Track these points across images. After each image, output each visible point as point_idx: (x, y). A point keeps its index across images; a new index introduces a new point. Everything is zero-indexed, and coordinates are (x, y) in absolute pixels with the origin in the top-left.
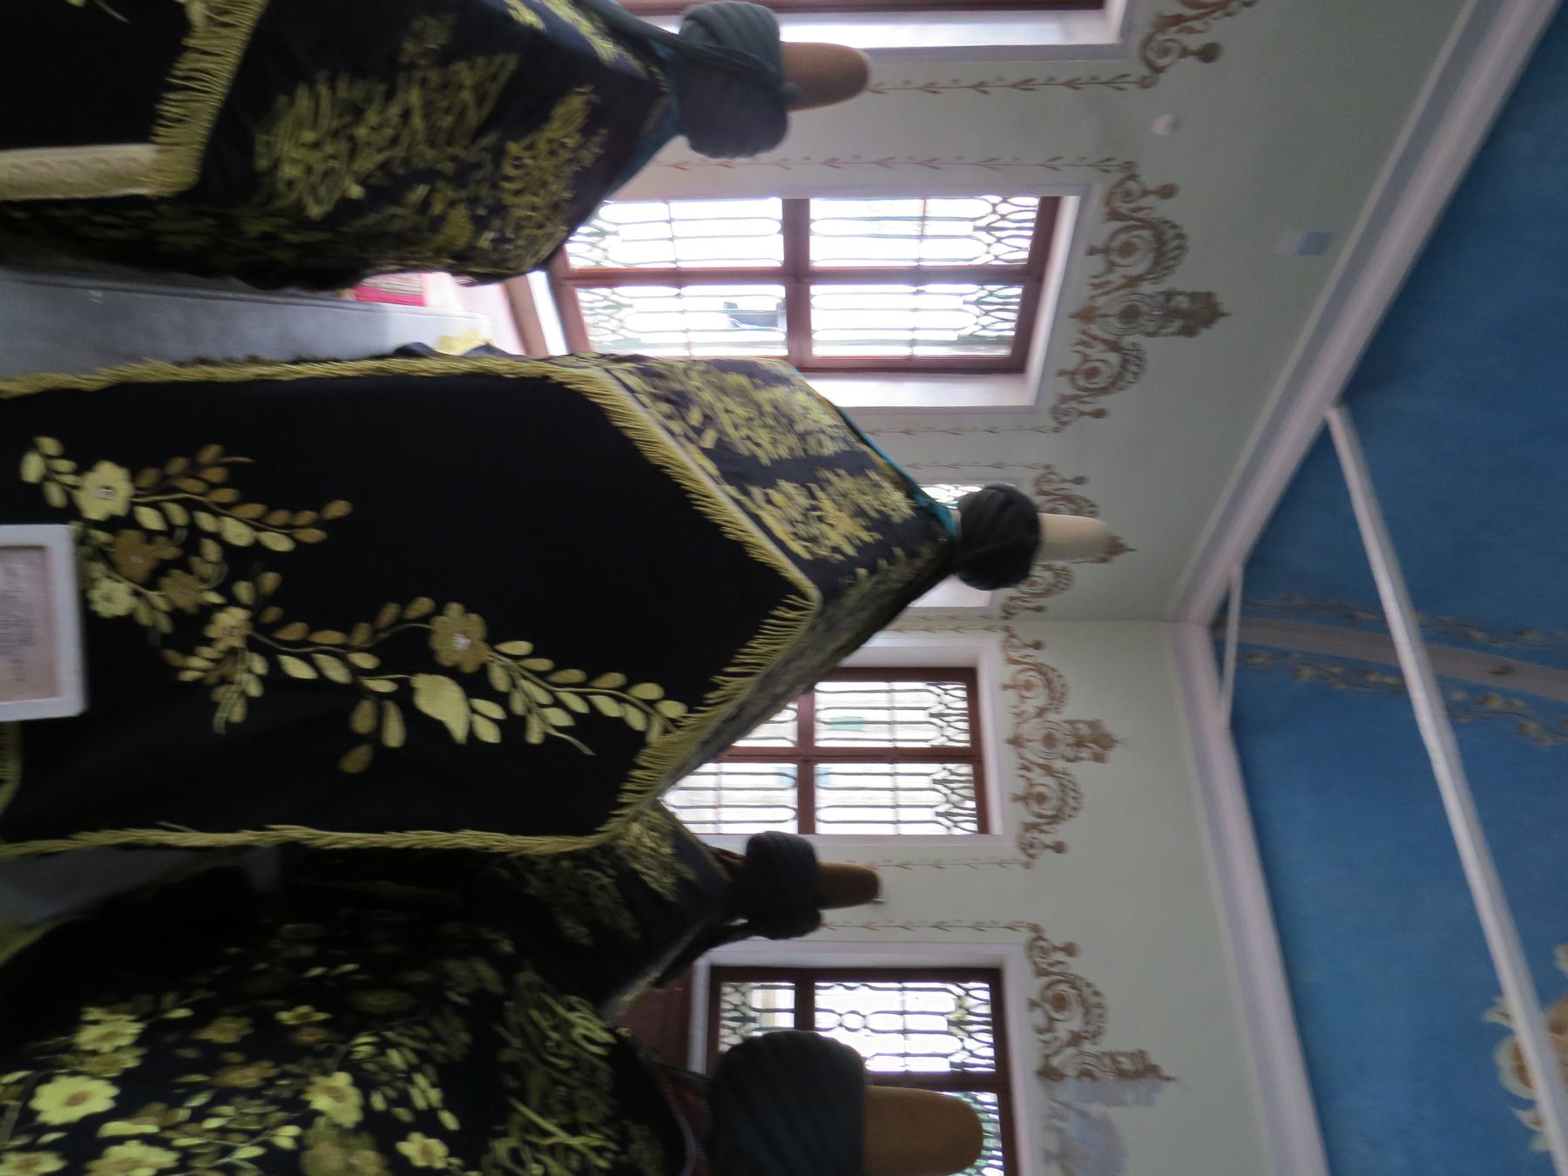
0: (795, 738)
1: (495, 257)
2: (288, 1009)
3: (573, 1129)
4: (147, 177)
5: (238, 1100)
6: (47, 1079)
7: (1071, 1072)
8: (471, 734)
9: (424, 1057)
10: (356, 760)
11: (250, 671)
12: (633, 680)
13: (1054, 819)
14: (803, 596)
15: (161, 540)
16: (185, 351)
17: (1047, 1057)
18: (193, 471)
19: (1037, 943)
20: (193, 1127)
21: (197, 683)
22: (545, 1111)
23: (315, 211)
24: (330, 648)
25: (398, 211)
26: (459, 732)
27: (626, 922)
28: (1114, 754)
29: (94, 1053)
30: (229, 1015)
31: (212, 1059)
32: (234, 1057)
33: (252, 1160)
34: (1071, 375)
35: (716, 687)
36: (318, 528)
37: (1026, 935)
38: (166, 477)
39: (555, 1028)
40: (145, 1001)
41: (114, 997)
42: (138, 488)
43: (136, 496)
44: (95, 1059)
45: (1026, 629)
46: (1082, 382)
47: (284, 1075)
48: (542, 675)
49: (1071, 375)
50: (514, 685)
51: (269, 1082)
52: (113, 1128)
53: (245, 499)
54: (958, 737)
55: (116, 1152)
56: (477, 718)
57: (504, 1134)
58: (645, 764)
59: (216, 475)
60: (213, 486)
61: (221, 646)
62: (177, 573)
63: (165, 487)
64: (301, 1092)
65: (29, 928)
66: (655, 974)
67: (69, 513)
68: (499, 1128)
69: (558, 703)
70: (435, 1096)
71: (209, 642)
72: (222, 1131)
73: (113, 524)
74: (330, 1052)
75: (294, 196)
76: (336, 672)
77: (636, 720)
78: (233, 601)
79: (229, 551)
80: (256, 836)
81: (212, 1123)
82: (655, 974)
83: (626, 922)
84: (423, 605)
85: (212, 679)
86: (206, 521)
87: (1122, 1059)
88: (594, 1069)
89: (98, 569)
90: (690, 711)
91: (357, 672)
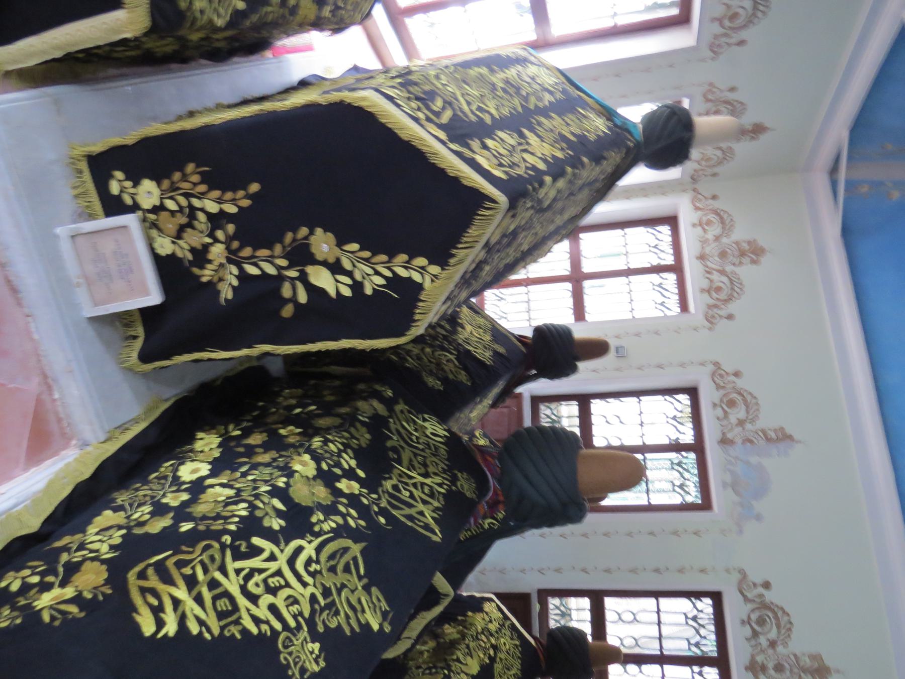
0: (570, 269)
1: (335, 20)
2: (284, 428)
3: (426, 475)
4: (126, 28)
5: (261, 468)
6: (183, 463)
7: (739, 440)
8: (338, 293)
9: (346, 446)
10: (287, 311)
11: (231, 273)
12: (412, 257)
13: (729, 299)
14: (494, 201)
15: (178, 215)
16: (182, 110)
17: (724, 434)
18: (185, 178)
19: (717, 372)
20: (243, 480)
21: (210, 283)
22: (411, 467)
23: (220, 22)
24: (265, 258)
25: (269, 9)
26: (332, 293)
27: (463, 377)
28: (764, 260)
29: (202, 452)
30: (258, 432)
31: (250, 451)
32: (260, 450)
33: (265, 492)
34: (720, 21)
35: (453, 256)
36: (248, 199)
37: (711, 367)
38: (173, 183)
39: (416, 430)
40: (222, 429)
41: (208, 427)
42: (161, 190)
43: (162, 194)
44: (202, 454)
45: (705, 187)
46: (727, 23)
47: (281, 456)
48: (367, 260)
49: (720, 21)
50: (354, 266)
51: (274, 460)
52: (209, 481)
53: (211, 189)
54: (669, 260)
55: (210, 490)
56: (339, 285)
57: (391, 478)
58: (424, 299)
59: (196, 178)
60: (195, 184)
61: (216, 263)
62: (189, 230)
63: (174, 188)
64: (289, 463)
65: (166, 400)
66: (488, 401)
67: (135, 207)
68: (387, 476)
69: (377, 273)
70: (353, 463)
71: (210, 262)
72: (254, 481)
73: (156, 210)
74: (301, 445)
75: (205, 18)
76: (271, 270)
77: (417, 277)
78: (216, 240)
79: (210, 216)
80: (249, 351)
81: (250, 478)
82: (488, 401)
83: (463, 377)
84: (304, 231)
85: (215, 279)
86: (196, 203)
87: (769, 432)
88: (436, 448)
89: (154, 233)
90: (443, 269)
91: (279, 268)
